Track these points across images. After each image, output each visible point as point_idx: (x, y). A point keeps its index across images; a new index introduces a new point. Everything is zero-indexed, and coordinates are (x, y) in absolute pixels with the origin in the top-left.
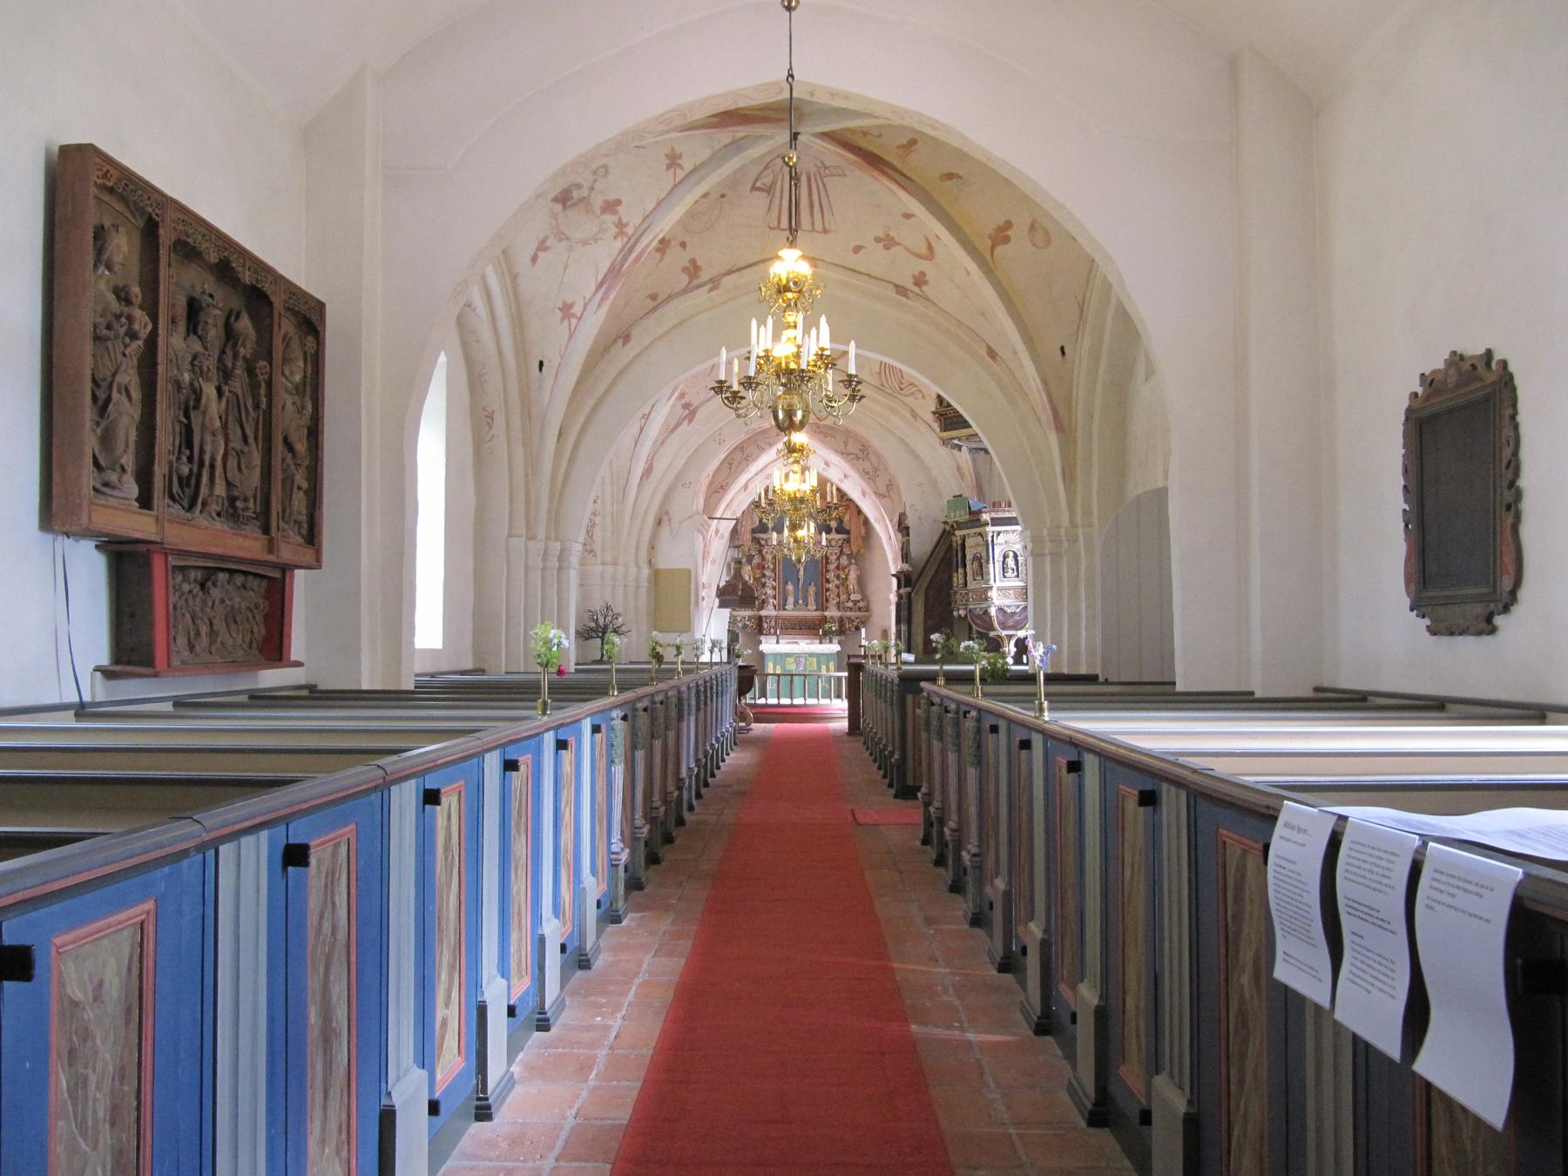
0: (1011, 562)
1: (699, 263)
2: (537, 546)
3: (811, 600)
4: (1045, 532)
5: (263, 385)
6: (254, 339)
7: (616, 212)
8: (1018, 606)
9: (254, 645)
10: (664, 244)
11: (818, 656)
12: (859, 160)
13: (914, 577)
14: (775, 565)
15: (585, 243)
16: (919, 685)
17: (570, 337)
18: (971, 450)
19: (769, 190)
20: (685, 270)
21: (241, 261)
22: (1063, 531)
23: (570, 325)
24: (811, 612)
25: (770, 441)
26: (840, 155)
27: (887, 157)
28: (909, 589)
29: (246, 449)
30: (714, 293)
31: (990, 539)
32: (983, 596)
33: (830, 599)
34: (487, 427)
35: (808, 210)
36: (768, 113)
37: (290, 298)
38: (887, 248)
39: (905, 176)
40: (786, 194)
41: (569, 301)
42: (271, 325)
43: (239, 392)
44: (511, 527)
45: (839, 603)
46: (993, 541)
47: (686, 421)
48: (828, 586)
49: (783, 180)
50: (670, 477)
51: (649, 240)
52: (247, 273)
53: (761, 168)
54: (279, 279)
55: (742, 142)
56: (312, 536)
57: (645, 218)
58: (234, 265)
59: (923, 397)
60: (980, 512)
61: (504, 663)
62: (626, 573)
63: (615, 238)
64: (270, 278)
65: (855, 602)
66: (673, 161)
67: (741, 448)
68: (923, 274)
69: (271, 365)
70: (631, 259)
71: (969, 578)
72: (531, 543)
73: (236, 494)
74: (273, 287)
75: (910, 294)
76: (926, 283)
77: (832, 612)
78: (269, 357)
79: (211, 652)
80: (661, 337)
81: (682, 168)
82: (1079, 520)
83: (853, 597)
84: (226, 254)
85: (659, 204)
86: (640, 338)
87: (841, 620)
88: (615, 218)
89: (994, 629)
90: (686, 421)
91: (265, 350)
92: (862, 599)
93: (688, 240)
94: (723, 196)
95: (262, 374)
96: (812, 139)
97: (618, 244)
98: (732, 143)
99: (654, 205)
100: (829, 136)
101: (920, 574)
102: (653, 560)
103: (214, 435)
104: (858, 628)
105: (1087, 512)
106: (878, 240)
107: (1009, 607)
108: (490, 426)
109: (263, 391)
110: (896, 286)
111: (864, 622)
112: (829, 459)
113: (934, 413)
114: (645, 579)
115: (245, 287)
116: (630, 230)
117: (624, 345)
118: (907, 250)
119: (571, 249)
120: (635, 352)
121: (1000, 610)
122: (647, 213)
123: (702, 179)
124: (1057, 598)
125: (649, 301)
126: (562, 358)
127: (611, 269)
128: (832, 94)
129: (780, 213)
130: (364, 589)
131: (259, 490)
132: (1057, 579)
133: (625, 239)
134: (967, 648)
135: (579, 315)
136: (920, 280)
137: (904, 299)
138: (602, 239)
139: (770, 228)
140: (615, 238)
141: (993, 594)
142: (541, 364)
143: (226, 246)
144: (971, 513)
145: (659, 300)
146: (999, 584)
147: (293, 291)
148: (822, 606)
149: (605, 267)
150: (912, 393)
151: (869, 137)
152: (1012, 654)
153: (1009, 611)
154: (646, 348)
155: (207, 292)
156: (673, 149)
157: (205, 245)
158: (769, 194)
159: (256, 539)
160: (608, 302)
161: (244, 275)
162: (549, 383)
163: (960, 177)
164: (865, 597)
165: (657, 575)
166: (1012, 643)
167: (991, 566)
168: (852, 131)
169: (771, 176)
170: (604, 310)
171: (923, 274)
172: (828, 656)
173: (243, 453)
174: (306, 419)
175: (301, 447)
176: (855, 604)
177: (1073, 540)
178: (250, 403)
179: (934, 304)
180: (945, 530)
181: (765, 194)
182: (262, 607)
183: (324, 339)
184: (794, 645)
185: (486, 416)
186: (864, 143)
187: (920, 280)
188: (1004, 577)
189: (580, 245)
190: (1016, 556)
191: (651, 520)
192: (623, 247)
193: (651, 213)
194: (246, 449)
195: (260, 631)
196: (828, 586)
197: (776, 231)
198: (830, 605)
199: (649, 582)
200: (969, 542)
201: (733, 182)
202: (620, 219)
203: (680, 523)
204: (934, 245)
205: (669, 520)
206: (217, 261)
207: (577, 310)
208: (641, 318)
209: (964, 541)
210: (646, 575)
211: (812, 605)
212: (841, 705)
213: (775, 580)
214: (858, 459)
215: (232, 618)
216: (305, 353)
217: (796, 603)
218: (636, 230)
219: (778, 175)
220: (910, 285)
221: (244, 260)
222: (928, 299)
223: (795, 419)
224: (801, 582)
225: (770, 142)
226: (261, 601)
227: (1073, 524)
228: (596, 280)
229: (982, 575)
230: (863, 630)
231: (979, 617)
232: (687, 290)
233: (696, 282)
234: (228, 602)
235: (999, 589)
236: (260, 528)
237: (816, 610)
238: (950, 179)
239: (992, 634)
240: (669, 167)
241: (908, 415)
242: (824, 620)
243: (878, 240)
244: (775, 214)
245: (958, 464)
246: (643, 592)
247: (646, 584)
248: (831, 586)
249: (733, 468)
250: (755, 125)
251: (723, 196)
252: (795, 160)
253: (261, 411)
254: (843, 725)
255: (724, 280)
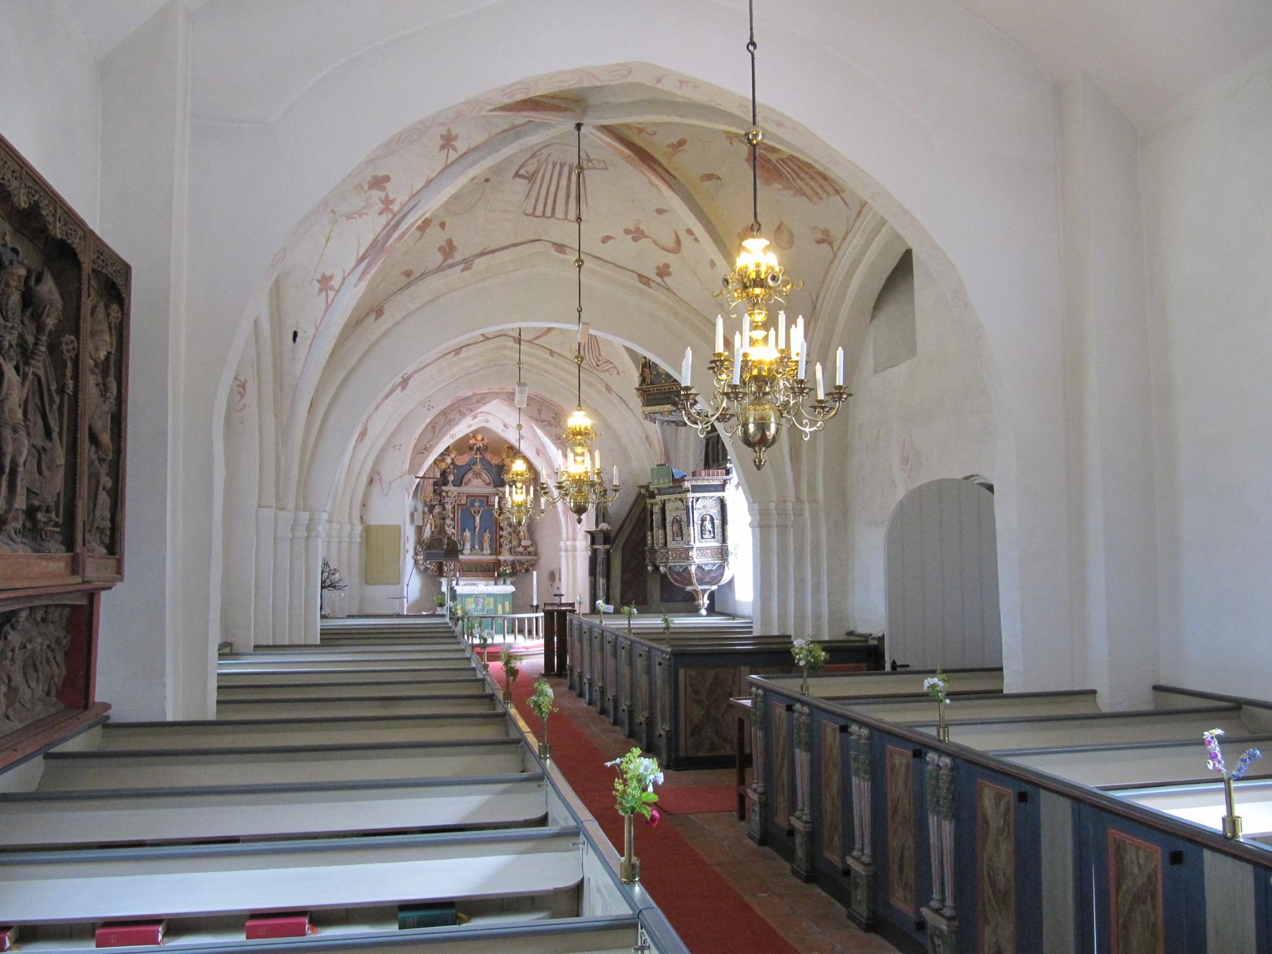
0: (708, 525)
1: (454, 244)
2: (286, 516)
3: (486, 545)
4: (773, 506)
5: (70, 364)
6: (60, 307)
7: (384, 189)
8: (714, 565)
9: (53, 692)
10: (424, 226)
11: (495, 596)
12: (633, 155)
13: (613, 535)
14: (454, 513)
15: (349, 217)
16: (1202, 851)
17: (327, 309)
18: (662, 423)
19: (531, 178)
20: (441, 249)
21: (51, 209)
22: (790, 506)
23: (327, 297)
24: (486, 556)
25: (471, 407)
26: (613, 147)
27: (656, 156)
28: (607, 547)
29: (48, 445)
30: (466, 273)
31: (690, 504)
32: (685, 554)
33: (504, 545)
34: (239, 397)
35: (564, 199)
36: (555, 102)
37: (98, 257)
38: (635, 239)
39: (667, 172)
40: (545, 185)
41: (328, 274)
42: (79, 290)
43: (41, 373)
44: (260, 499)
45: (510, 548)
46: (692, 506)
47: (400, 388)
48: (501, 533)
49: (545, 170)
50: (382, 440)
51: (415, 218)
52: (58, 225)
53: (528, 156)
54: (88, 234)
55: (520, 129)
56: (113, 546)
57: (413, 196)
58: (44, 213)
59: (618, 373)
60: (682, 479)
61: (252, 637)
62: (340, 530)
63: (380, 214)
64: (80, 233)
65: (526, 548)
66: (448, 141)
67: (444, 413)
68: (667, 266)
69: (78, 339)
70: (396, 235)
71: (669, 538)
72: (281, 514)
73: (37, 503)
74: (82, 243)
75: (652, 284)
76: (669, 274)
77: (505, 556)
78: (76, 332)
79: (8, 718)
80: (411, 313)
81: (455, 150)
82: (805, 497)
83: (524, 543)
84: (36, 198)
85: (428, 183)
86: (392, 314)
87: (513, 563)
88: (382, 195)
89: (691, 584)
90: (400, 388)
91: (73, 323)
92: (531, 545)
93: (446, 220)
94: (487, 180)
95: (68, 351)
96: (594, 131)
97: (383, 219)
98: (509, 129)
99: (423, 183)
100: (607, 129)
101: (618, 533)
102: (365, 517)
103: (15, 431)
104: (527, 570)
105: (812, 489)
106: (627, 232)
107: (707, 565)
108: (242, 396)
109: (69, 373)
110: (639, 275)
111: (532, 566)
112: (507, 421)
113: (638, 389)
114: (358, 536)
115: (54, 240)
116: (395, 207)
117: (376, 319)
118: (655, 242)
119: (334, 222)
120: (384, 328)
121: (699, 567)
122: (414, 192)
123: (475, 162)
124: (783, 566)
125: (404, 277)
126: (317, 329)
127: (374, 244)
128: (681, 82)
129: (537, 200)
130: (168, 593)
131: (62, 497)
132: (783, 550)
133: (390, 216)
134: (933, 686)
135: (337, 288)
136: (663, 271)
137: (646, 288)
138: (367, 214)
139: (526, 214)
140: (380, 214)
141: (693, 554)
142: (295, 334)
143: (37, 188)
144: (674, 480)
145: (413, 277)
146: (698, 545)
147: (102, 250)
148: (496, 550)
149: (366, 243)
150: (608, 370)
151: (644, 134)
152: (706, 606)
153: (707, 569)
154: (398, 322)
155: (10, 246)
156: (449, 130)
157: (15, 184)
158: (530, 182)
159: (60, 559)
160: (369, 277)
161: (55, 227)
162: (302, 353)
163: (719, 178)
164: (534, 543)
165: (367, 530)
166: (706, 596)
167: (691, 528)
168: (629, 126)
169: (536, 165)
170: (363, 285)
171: (667, 266)
172: (504, 596)
173: (44, 449)
174: (109, 406)
175: (105, 438)
176: (526, 549)
177: (799, 514)
178: (54, 387)
179: (673, 293)
180: (640, 493)
181: (527, 181)
182: (64, 642)
183: (129, 309)
184: (473, 587)
185: (238, 386)
186: (636, 139)
187: (663, 271)
188: (702, 538)
189: (344, 218)
190: (712, 519)
191: (364, 479)
192: (388, 224)
193: (418, 192)
194: (48, 445)
195: (58, 672)
196: (501, 533)
197: (542, 219)
198: (503, 550)
199: (361, 537)
200: (668, 506)
201: (498, 169)
202: (387, 196)
203: (391, 483)
204: (682, 239)
205: (380, 480)
206: (26, 206)
207: (336, 283)
208: (394, 294)
209: (664, 505)
210: (359, 532)
211: (487, 551)
212: (538, 644)
213: (454, 528)
214: (551, 425)
215: (31, 665)
216: (110, 323)
217: (473, 547)
218: (401, 209)
219: (542, 163)
220: (652, 274)
221: (55, 208)
222: (668, 289)
223: (768, 433)
224: (477, 530)
225: (553, 130)
226: (61, 634)
227: (798, 499)
228: (358, 254)
229: (682, 536)
230: (535, 573)
231: (678, 573)
232: (440, 269)
233: (450, 261)
234: (29, 646)
235: (698, 549)
236: (62, 543)
237: (490, 554)
238: (710, 179)
239: (689, 588)
240: (442, 147)
241: (603, 389)
242: (498, 564)
243: (627, 232)
244: (532, 201)
245: (646, 433)
246: (356, 548)
247: (359, 540)
248: (504, 533)
249: (437, 432)
250: (546, 113)
251: (487, 180)
252: (760, 138)
253: (66, 398)
254: (540, 660)
255: (477, 261)
